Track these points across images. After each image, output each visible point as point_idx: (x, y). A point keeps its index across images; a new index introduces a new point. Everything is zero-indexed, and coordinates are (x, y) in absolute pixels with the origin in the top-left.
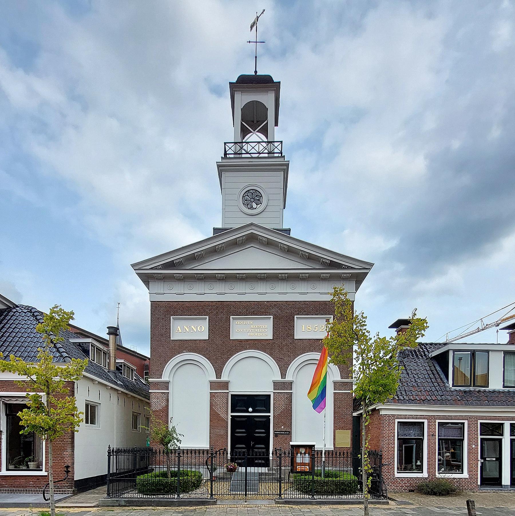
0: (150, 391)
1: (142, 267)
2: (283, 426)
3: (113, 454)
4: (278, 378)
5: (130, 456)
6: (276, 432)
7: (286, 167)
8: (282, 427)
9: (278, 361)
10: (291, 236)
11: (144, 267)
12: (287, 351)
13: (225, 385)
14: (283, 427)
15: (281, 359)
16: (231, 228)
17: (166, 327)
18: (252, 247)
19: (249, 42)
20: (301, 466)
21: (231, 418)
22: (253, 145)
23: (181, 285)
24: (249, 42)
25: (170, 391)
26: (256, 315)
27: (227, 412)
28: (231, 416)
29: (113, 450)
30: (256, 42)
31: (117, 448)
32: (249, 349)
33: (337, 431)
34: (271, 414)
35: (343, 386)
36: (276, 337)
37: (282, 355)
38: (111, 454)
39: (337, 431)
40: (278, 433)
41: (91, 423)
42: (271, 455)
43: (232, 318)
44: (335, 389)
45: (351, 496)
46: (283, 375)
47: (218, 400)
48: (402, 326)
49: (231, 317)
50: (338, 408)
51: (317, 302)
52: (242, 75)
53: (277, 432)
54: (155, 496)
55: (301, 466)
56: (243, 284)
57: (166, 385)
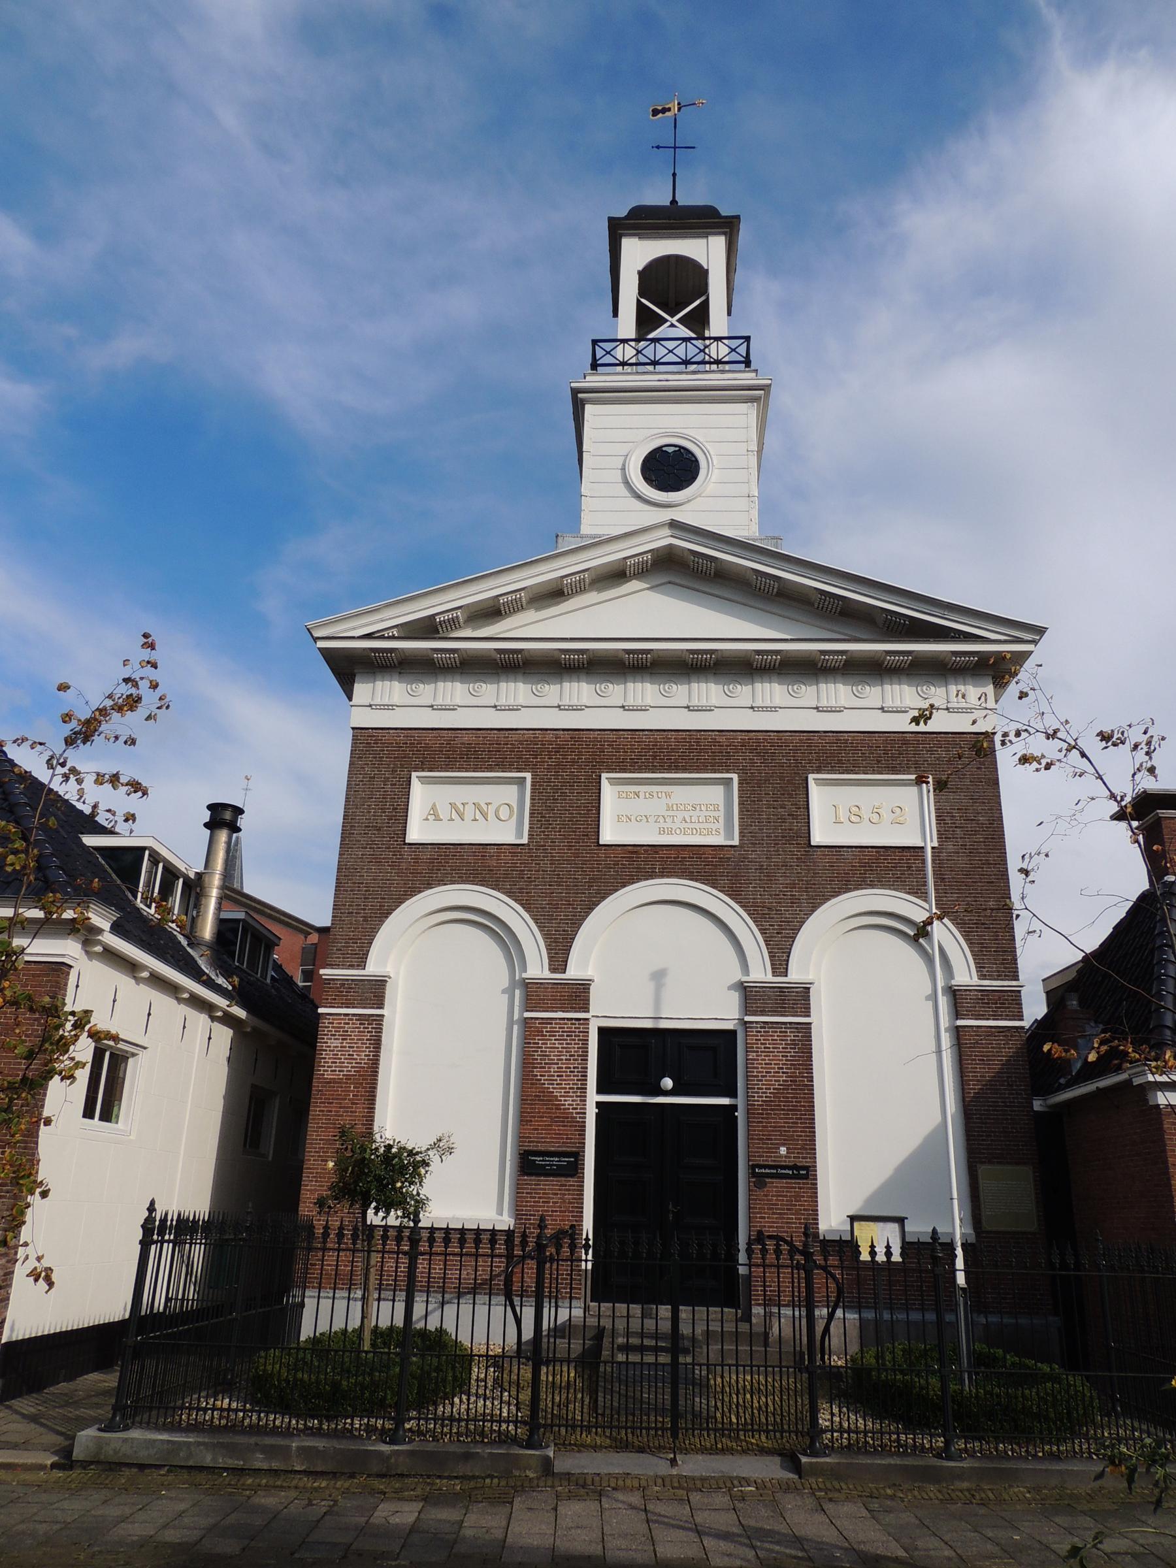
0: (321, 1010)
1: (345, 631)
2: (784, 1145)
3: (163, 1238)
4: (760, 972)
5: (849, 1238)
6: (760, 1167)
7: (762, 392)
9: (758, 913)
11: (354, 629)
13: (578, 995)
14: (783, 1150)
19: (658, 147)
21: (597, 1110)
24: (658, 147)
26: (677, 769)
27: (583, 1089)
28: (599, 1104)
29: (164, 1221)
30: (675, 148)
31: (224, 1214)
32: (663, 877)
34: (740, 1102)
38: (155, 1237)
39: (982, 1169)
40: (767, 1171)
41: (101, 1119)
42: (742, 1257)
45: (272, 1417)
47: (552, 1046)
48: (1158, 811)
51: (877, 735)
52: (633, 208)
53: (765, 1167)
54: (942, 1442)
56: (628, 684)
57: (376, 991)
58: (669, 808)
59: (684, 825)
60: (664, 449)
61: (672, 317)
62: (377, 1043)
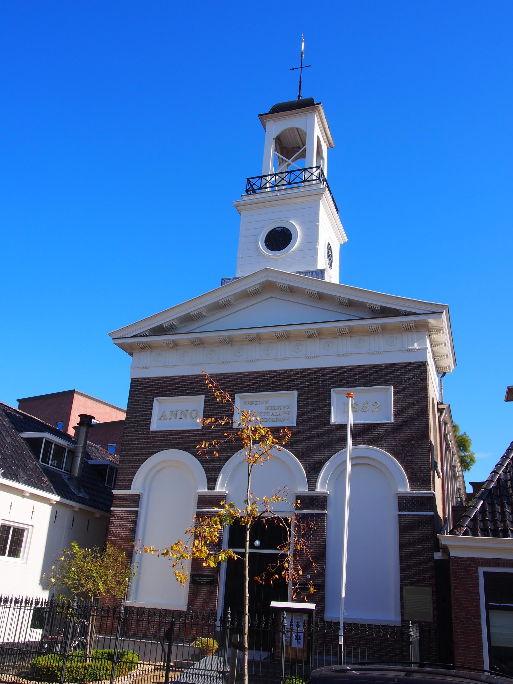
0: (112, 509)
2: (309, 574)
8: (308, 576)
10: (326, 280)
12: (319, 444)
15: (309, 457)
16: (239, 278)
17: (146, 413)
18: (271, 297)
19: (293, 69)
20: (96, 616)
22: (297, 173)
23: (151, 353)
24: (293, 69)
25: (142, 510)
33: (405, 588)
35: (414, 503)
36: (301, 423)
37: (310, 450)
43: (156, 400)
44: (400, 510)
46: (312, 484)
49: (236, 395)
50: (407, 543)
55: (96, 616)
57: (135, 500)
58: (267, 409)
59: (273, 417)
60: (276, 229)
61: (289, 159)
62: (135, 524)
